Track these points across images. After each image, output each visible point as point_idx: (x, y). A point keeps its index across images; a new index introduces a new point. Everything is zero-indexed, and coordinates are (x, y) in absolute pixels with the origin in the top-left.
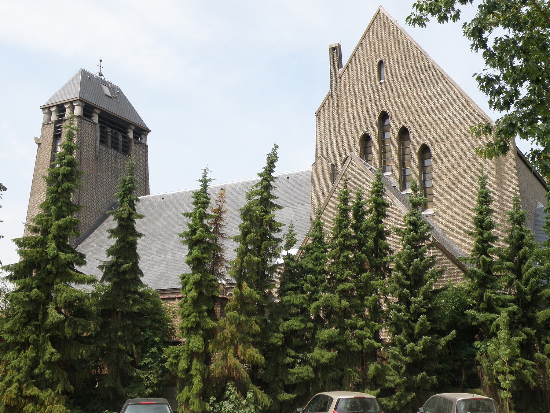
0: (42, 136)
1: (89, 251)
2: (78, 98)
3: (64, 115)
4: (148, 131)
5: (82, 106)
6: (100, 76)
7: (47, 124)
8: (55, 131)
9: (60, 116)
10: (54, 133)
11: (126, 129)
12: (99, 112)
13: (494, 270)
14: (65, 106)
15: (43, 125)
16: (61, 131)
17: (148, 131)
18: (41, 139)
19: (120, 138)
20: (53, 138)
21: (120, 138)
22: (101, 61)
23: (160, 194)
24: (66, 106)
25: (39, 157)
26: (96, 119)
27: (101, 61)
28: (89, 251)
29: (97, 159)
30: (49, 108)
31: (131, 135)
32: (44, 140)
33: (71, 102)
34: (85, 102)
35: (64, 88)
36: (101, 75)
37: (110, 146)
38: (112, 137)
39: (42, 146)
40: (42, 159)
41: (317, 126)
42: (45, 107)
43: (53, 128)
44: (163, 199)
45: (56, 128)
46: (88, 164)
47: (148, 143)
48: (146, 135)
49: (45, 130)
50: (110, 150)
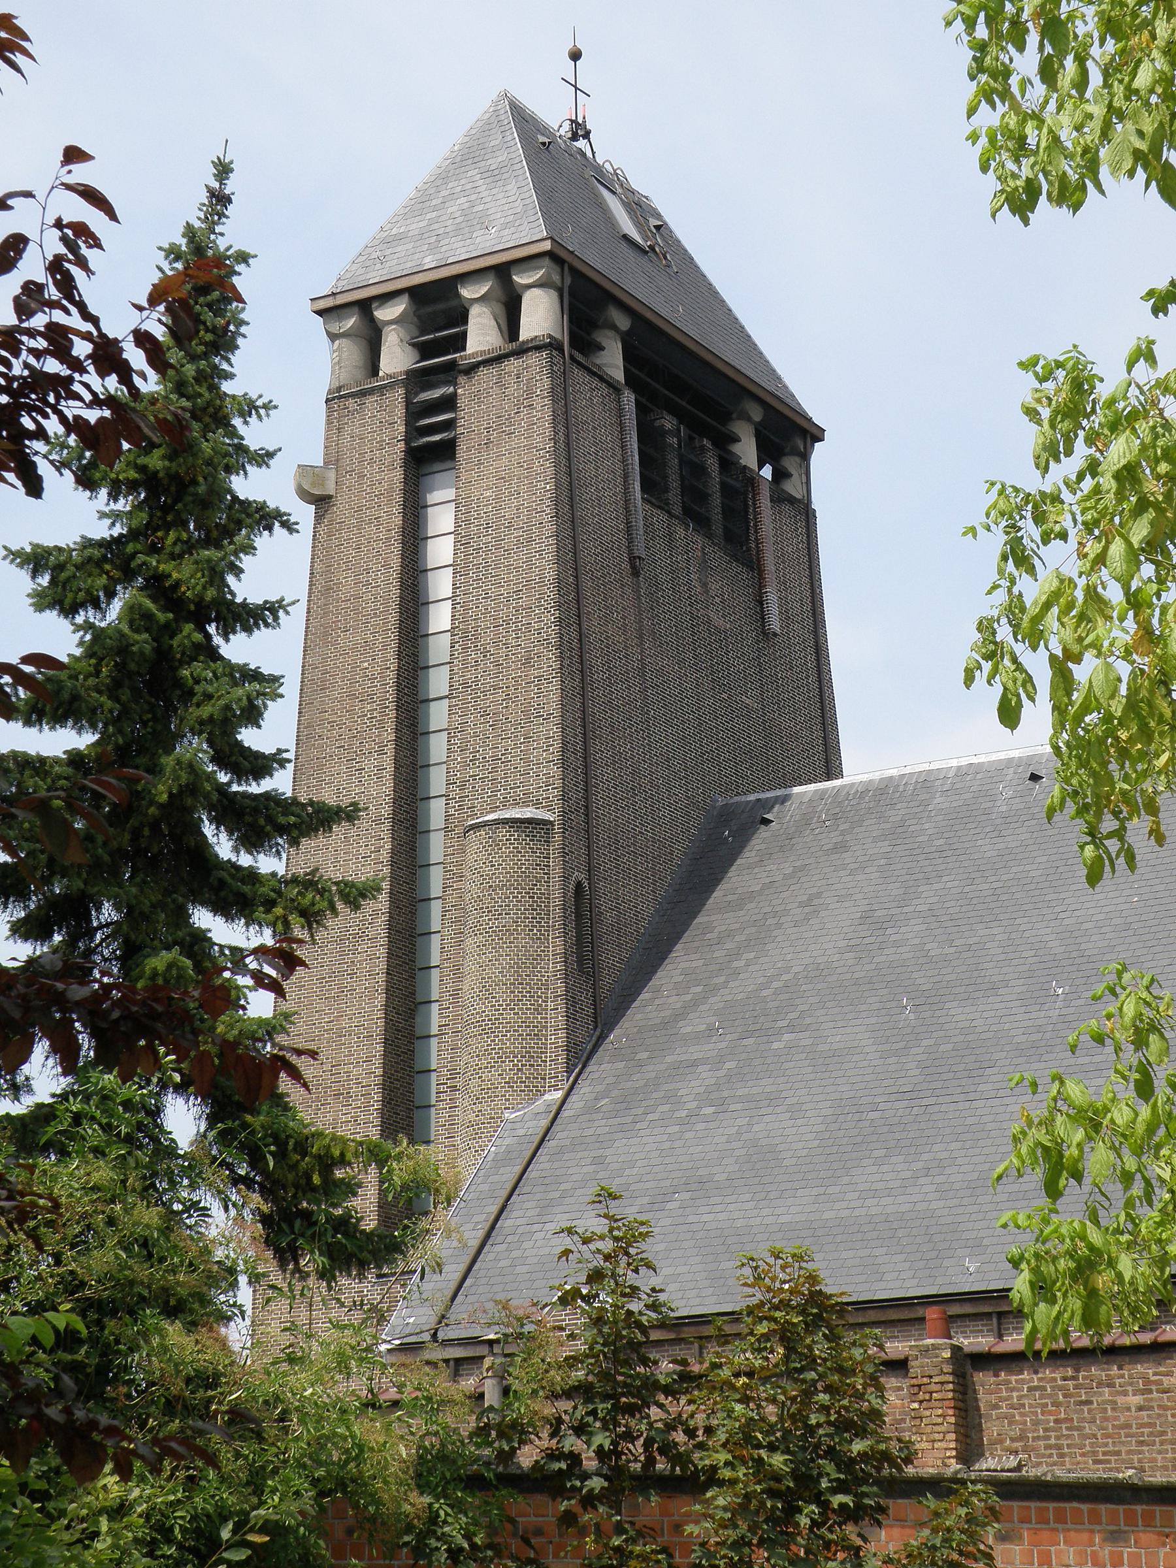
0: (333, 458)
1: (694, 1064)
2: (547, 246)
3: (459, 341)
4: (814, 435)
5: (560, 291)
6: (575, 137)
7: (363, 394)
8: (413, 431)
9: (425, 350)
10: (407, 441)
11: (726, 417)
12: (624, 323)
13: (60, 1304)
14: (516, 278)
15: (335, 398)
16: (449, 425)
17: (814, 435)
18: (332, 475)
19: (712, 462)
20: (406, 465)
21: (712, 462)
22: (576, 56)
23: (1002, 756)
24: (467, 292)
25: (328, 570)
26: (613, 360)
27: (576, 56)
28: (694, 1064)
29: (635, 573)
30: (365, 306)
31: (747, 451)
32: (348, 481)
33: (502, 272)
34: (574, 271)
35: (422, 202)
36: (579, 130)
37: (677, 510)
38: (682, 461)
39: (341, 508)
40: (345, 579)
41: (307, 628)
42: (340, 300)
43: (400, 411)
44: (1035, 778)
45: (414, 412)
46: (605, 600)
47: (818, 502)
48: (805, 457)
49: (353, 428)
50: (680, 532)
